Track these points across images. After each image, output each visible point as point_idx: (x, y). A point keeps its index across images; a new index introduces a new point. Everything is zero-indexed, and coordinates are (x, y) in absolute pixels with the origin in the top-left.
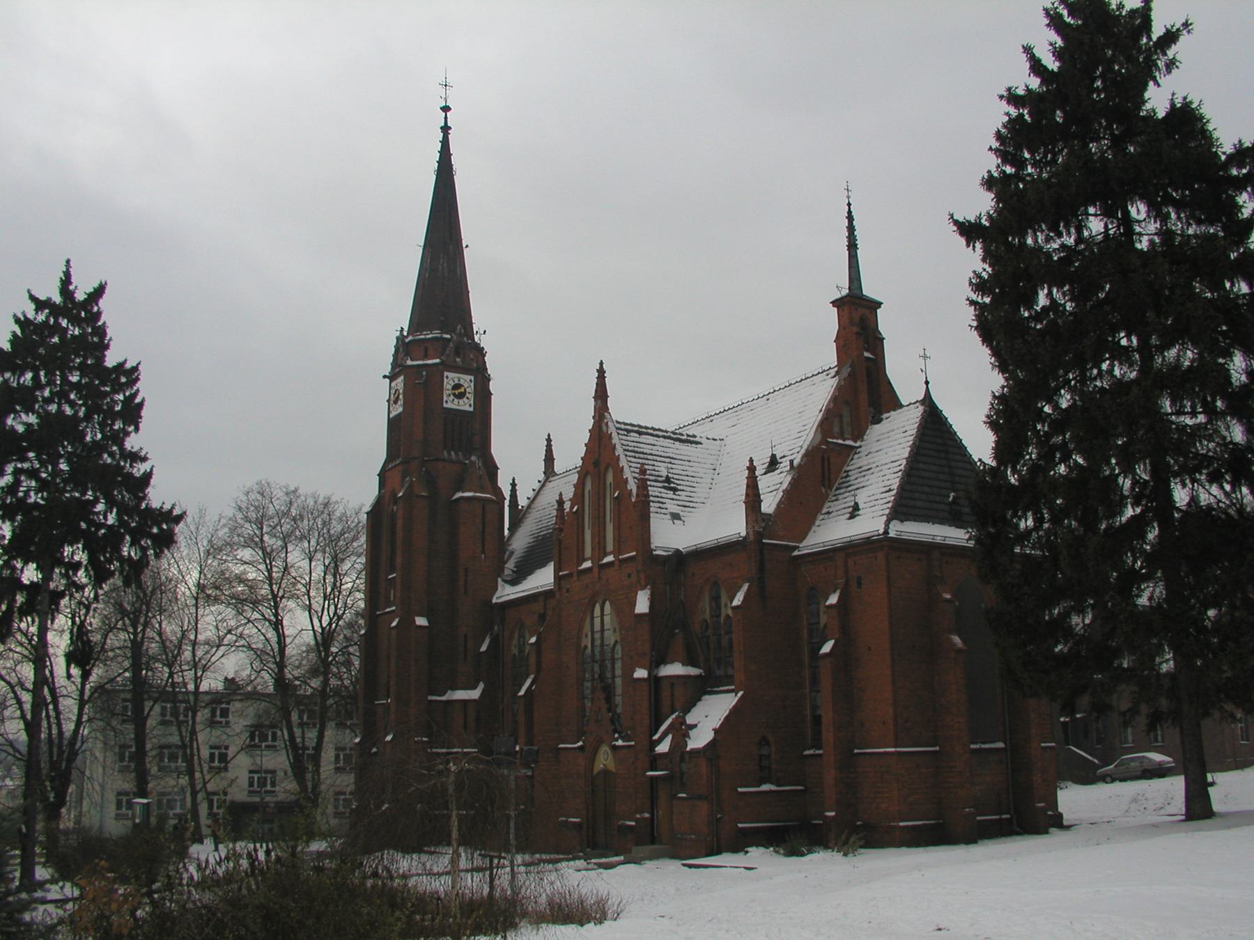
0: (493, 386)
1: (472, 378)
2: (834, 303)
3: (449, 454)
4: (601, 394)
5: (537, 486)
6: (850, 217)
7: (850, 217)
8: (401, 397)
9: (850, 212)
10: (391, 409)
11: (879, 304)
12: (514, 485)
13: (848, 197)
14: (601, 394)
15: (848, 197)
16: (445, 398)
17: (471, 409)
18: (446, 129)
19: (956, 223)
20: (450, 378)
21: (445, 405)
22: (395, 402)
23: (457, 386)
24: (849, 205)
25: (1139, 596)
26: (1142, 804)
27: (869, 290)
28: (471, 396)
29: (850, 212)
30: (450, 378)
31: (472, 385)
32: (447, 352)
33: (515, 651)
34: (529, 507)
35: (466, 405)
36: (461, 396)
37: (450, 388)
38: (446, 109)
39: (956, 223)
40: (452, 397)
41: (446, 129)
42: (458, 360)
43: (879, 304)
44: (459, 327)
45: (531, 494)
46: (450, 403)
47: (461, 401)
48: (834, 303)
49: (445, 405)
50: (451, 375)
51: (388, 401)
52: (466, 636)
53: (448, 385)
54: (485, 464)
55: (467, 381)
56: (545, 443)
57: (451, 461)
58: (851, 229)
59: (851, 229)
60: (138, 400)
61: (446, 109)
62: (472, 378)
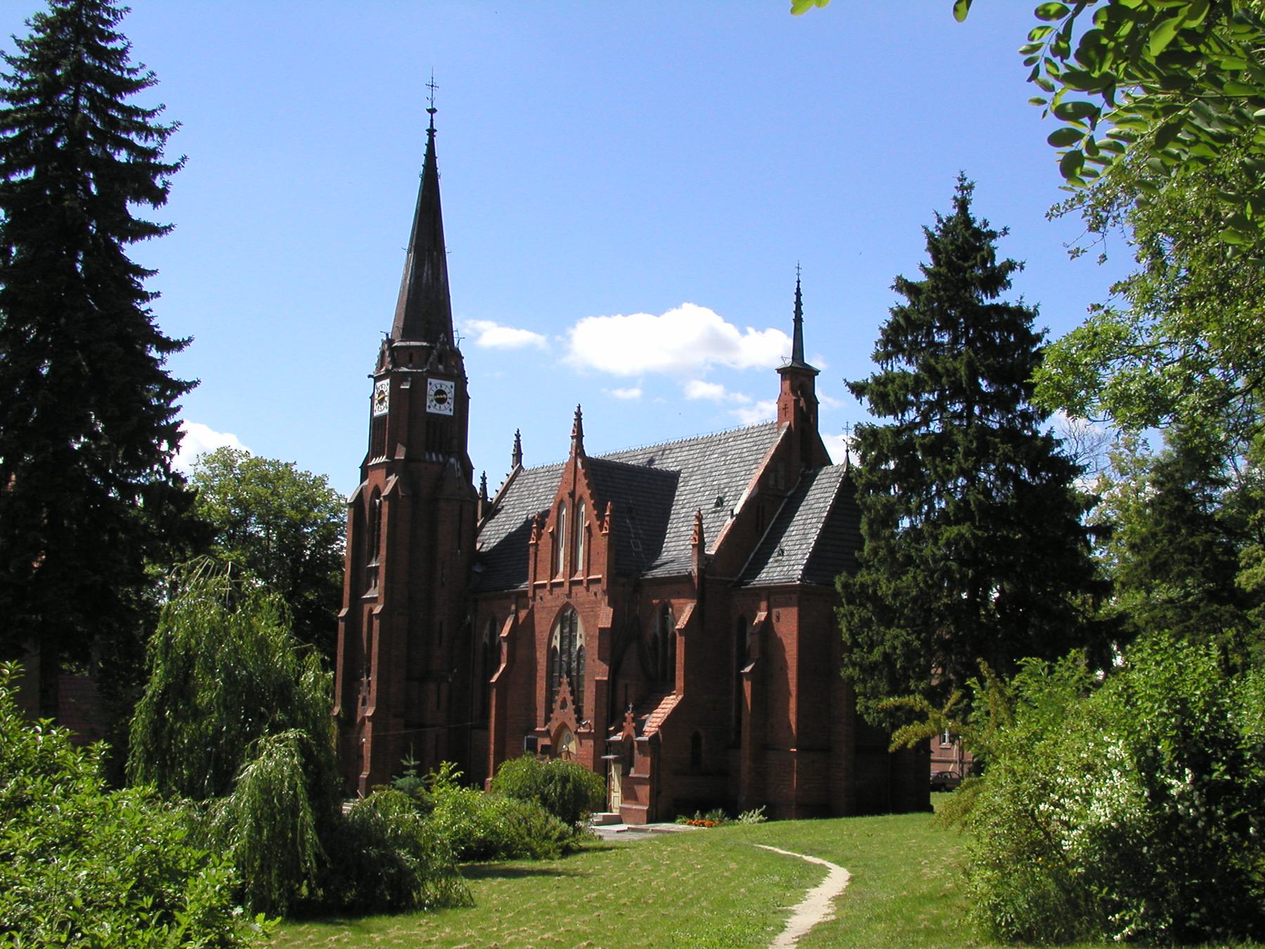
0: (470, 389)
1: (453, 384)
2: (779, 371)
3: (431, 456)
4: (578, 435)
5: (506, 480)
6: (798, 294)
7: (798, 294)
8: (386, 399)
9: (798, 289)
10: (375, 408)
11: (817, 372)
12: (484, 478)
13: (798, 275)
14: (578, 435)
15: (798, 275)
16: (428, 404)
17: (452, 414)
18: (431, 132)
19: (848, 384)
20: (434, 385)
21: (428, 410)
22: (381, 401)
23: (440, 392)
24: (799, 282)
25: (1234, 493)
26: (671, 868)
27: (811, 360)
28: (451, 401)
29: (798, 289)
30: (434, 385)
31: (453, 390)
32: (431, 359)
33: (486, 640)
34: (499, 500)
35: (447, 410)
36: (441, 401)
37: (433, 393)
38: (432, 111)
39: (848, 384)
40: (434, 402)
41: (431, 132)
42: (441, 367)
43: (817, 372)
44: (442, 336)
45: (500, 488)
46: (433, 408)
47: (442, 406)
48: (779, 371)
49: (428, 410)
50: (434, 381)
51: (372, 397)
52: (441, 623)
53: (431, 391)
54: (462, 465)
55: (448, 386)
56: (515, 438)
57: (432, 462)
58: (798, 304)
59: (798, 304)
60: (180, 430)
61: (432, 111)
62: (453, 384)
